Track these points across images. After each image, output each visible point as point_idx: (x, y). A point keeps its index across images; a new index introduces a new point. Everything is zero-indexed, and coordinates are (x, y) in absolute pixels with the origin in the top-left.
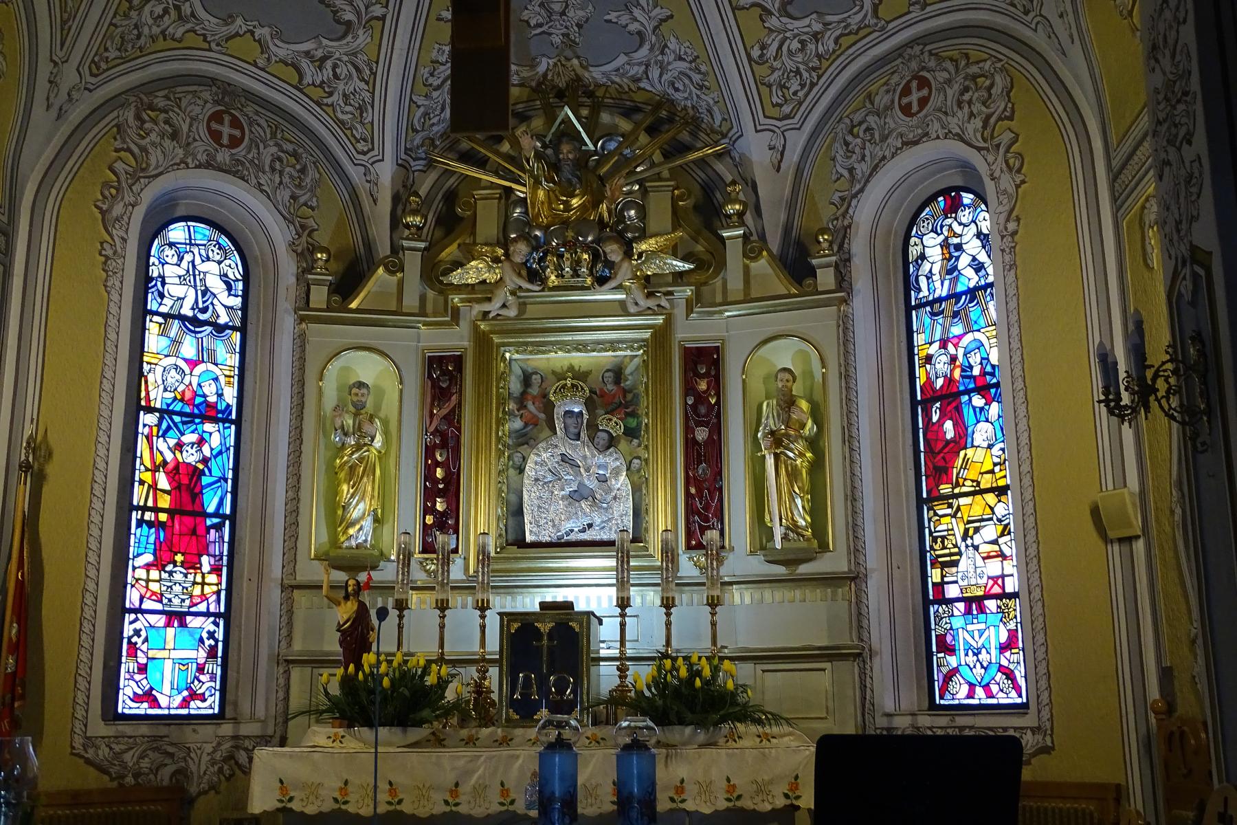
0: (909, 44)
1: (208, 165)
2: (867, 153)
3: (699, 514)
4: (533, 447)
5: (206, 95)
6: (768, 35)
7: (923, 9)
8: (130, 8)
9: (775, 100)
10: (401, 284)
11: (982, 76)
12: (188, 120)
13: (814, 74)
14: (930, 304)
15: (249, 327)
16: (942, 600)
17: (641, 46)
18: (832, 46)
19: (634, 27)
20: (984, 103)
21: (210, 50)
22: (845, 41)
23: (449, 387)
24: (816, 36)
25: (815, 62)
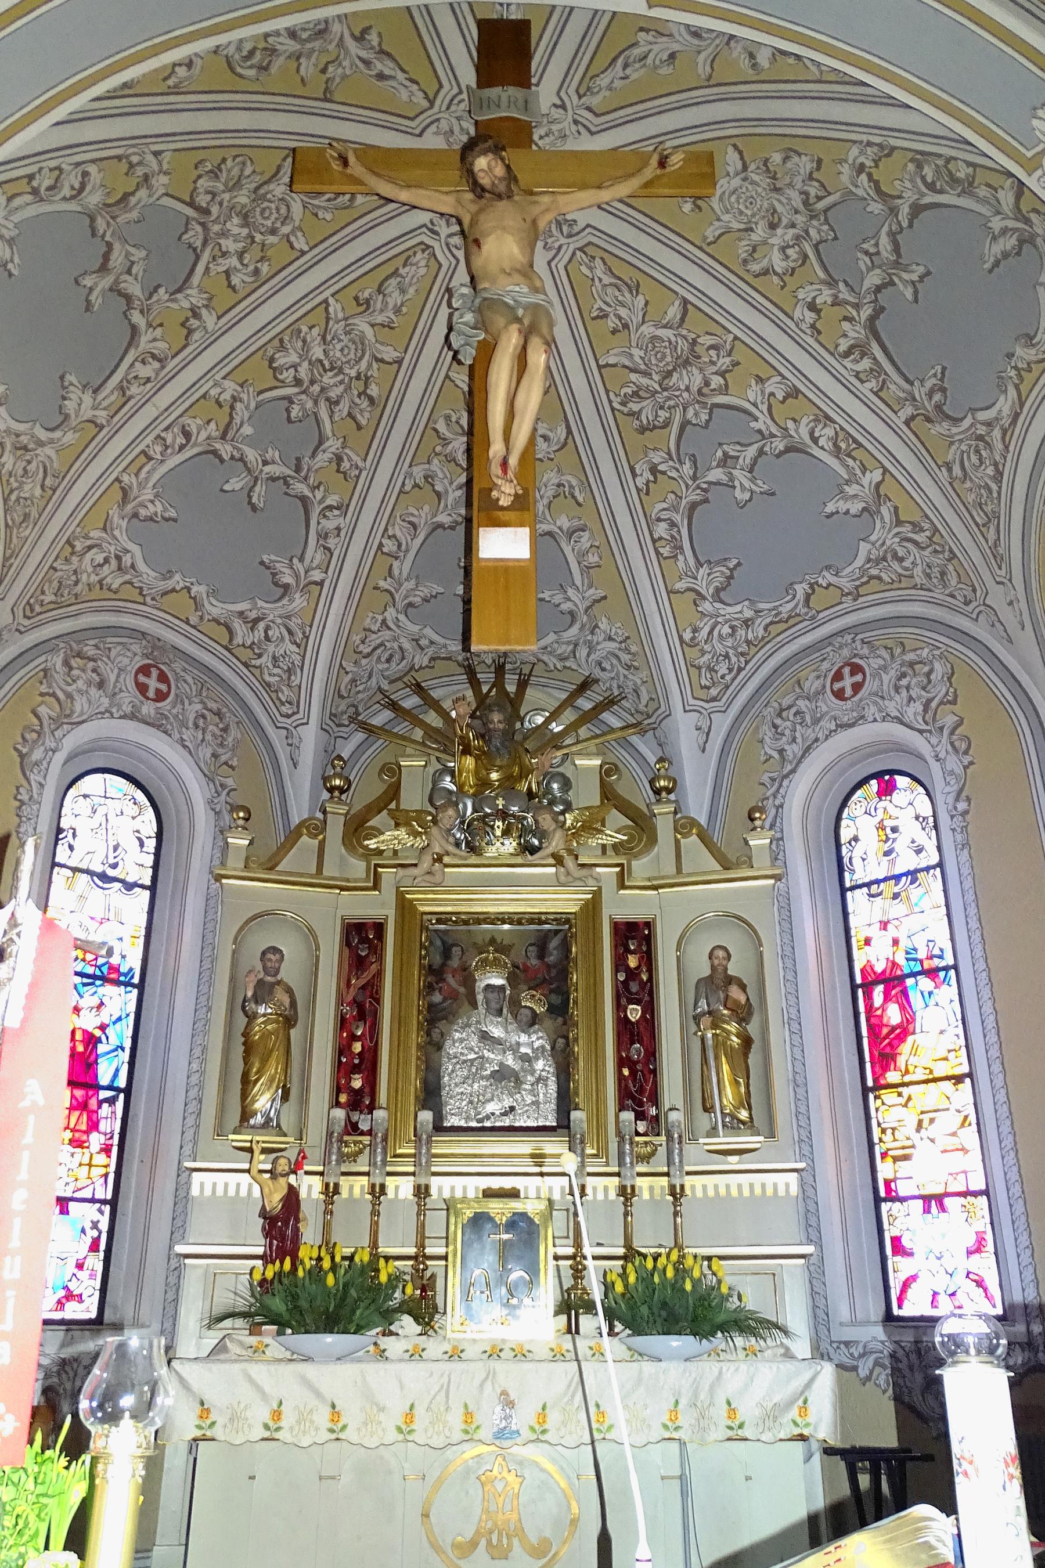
0: (840, 633)
1: (132, 716)
2: (798, 735)
3: (634, 1099)
4: (452, 1023)
5: (136, 648)
6: (701, 620)
7: (855, 600)
8: (73, 553)
9: (704, 682)
10: (322, 845)
11: (920, 662)
12: (116, 671)
13: (742, 659)
14: (868, 885)
15: (159, 886)
16: (892, 1197)
17: (571, 626)
18: (761, 633)
19: (566, 606)
20: (924, 688)
21: (144, 604)
22: (774, 629)
23: (367, 956)
24: (747, 623)
25: (744, 648)
